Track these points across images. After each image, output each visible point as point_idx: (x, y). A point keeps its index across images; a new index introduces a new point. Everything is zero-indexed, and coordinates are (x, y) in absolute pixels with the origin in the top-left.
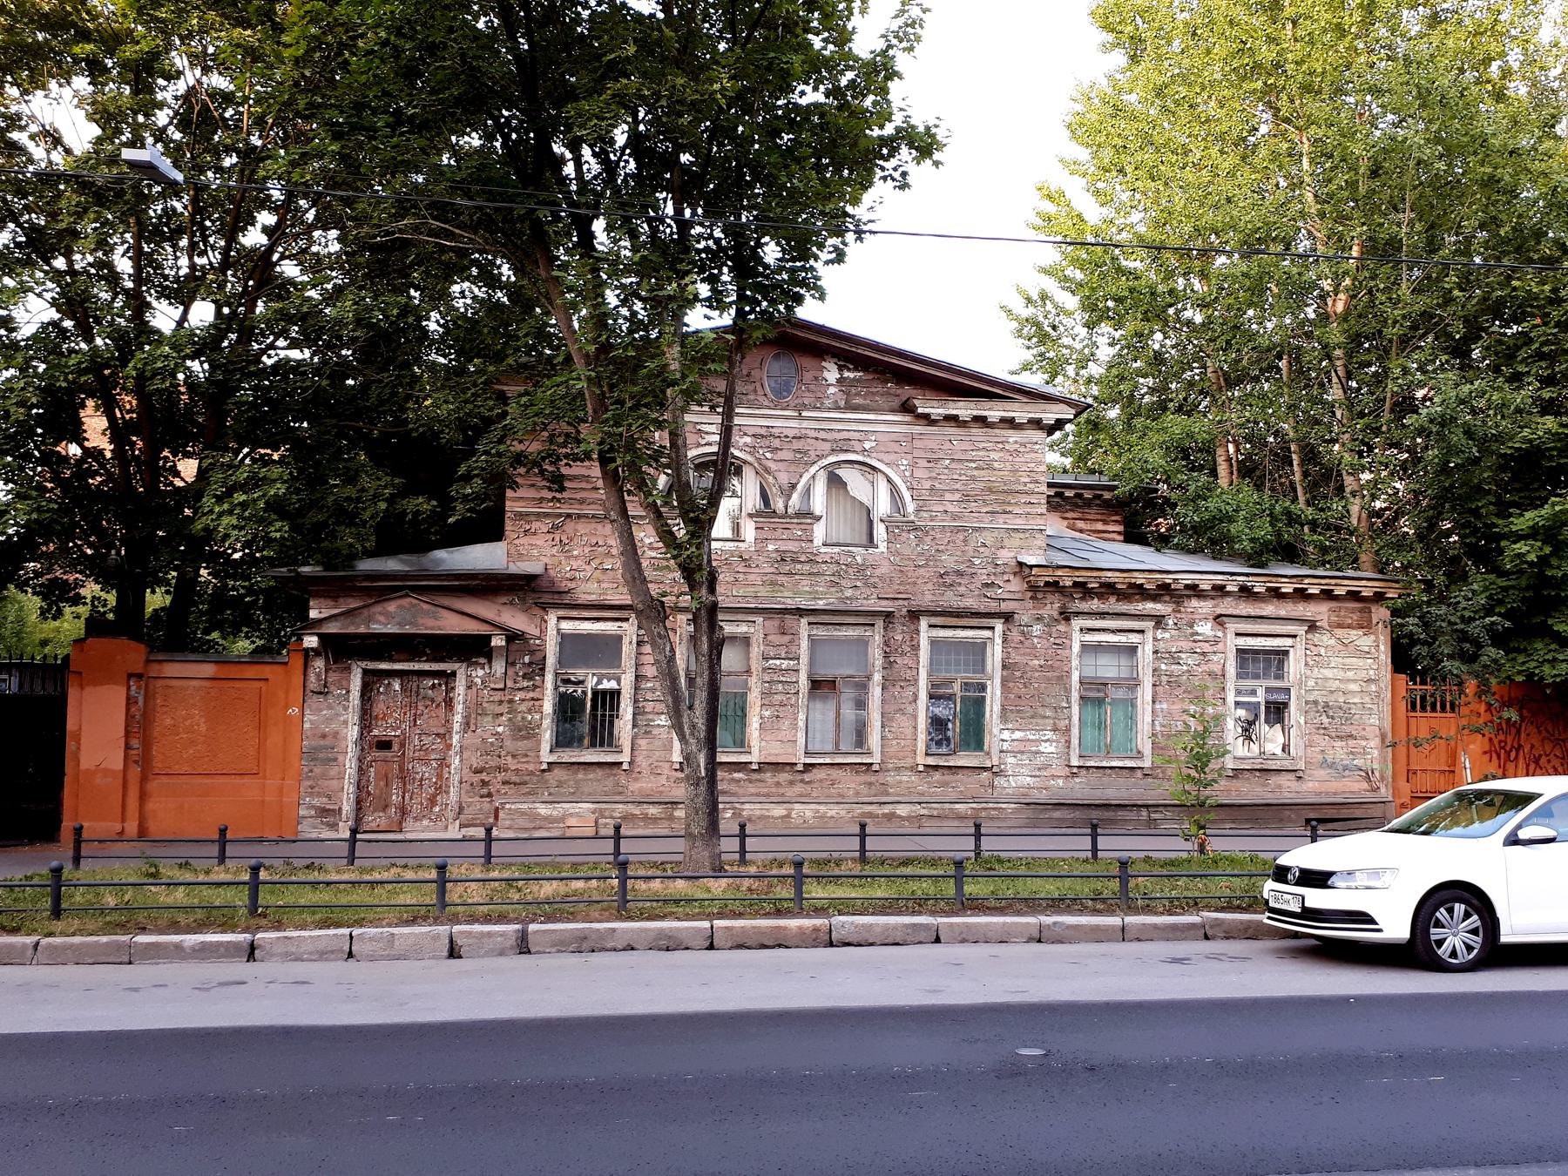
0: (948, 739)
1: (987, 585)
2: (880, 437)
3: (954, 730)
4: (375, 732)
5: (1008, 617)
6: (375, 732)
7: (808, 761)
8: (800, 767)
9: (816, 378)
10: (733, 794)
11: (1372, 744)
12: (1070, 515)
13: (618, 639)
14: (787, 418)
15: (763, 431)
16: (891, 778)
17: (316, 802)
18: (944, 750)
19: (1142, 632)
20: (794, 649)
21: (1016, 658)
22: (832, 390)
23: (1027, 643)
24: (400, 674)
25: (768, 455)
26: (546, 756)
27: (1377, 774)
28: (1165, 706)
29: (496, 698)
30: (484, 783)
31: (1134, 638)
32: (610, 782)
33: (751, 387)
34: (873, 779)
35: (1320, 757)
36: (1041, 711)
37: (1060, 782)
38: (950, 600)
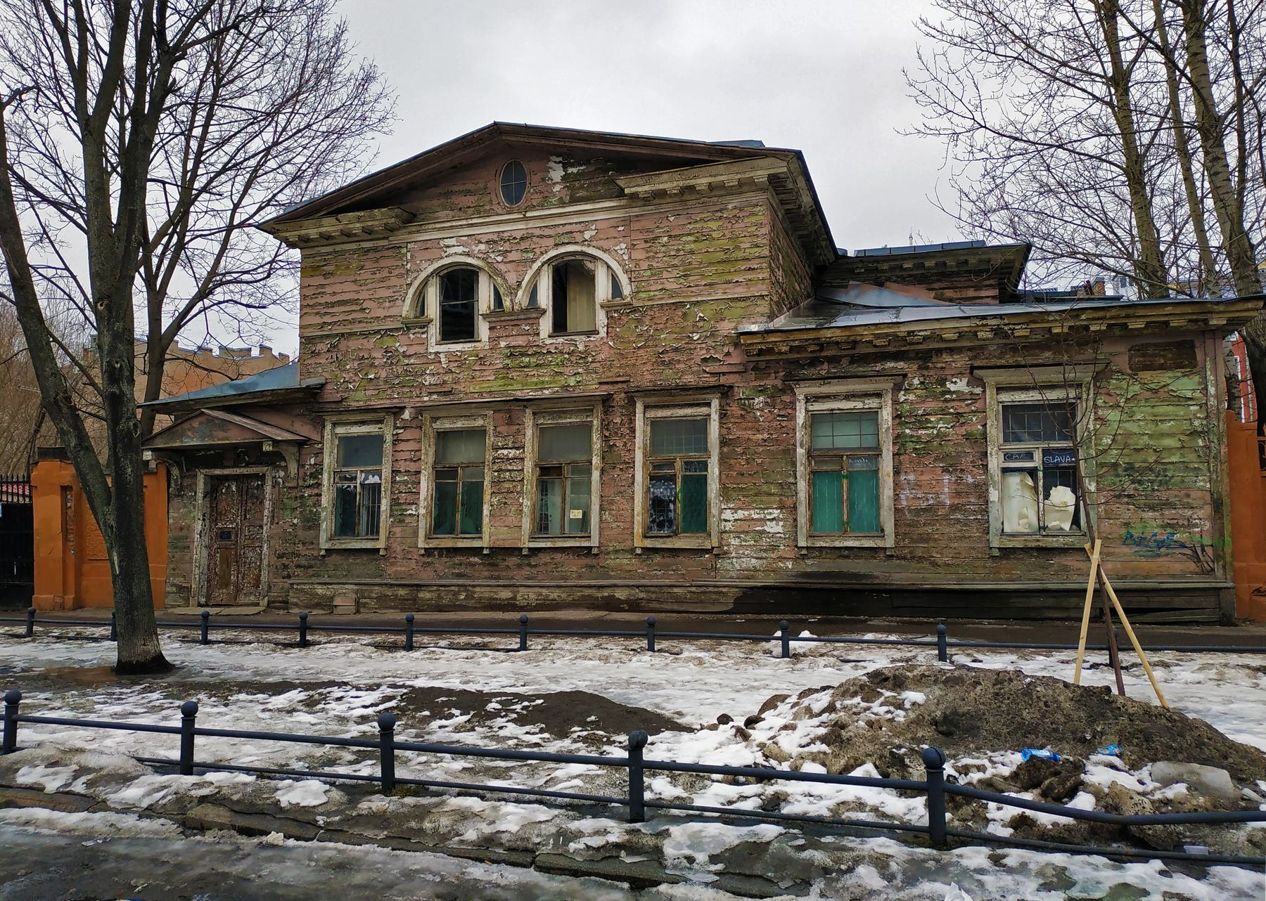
0: (670, 522)
1: (705, 360)
2: (601, 225)
3: (677, 510)
4: (220, 525)
5: (725, 392)
6: (220, 525)
7: (532, 545)
8: (525, 552)
9: (543, 180)
10: (469, 578)
11: (1201, 513)
12: (936, 285)
13: (380, 439)
14: (514, 221)
15: (495, 237)
16: (611, 561)
17: (177, 581)
18: (665, 532)
19: (878, 395)
20: (520, 438)
21: (736, 433)
22: (557, 188)
23: (748, 417)
24: (236, 478)
25: (500, 259)
26: (324, 544)
27: (1209, 551)
28: (911, 477)
29: (293, 494)
30: (285, 567)
31: (872, 403)
32: (372, 566)
33: (487, 199)
34: (594, 562)
35: (1123, 531)
36: (765, 488)
37: (790, 565)
38: (669, 377)
